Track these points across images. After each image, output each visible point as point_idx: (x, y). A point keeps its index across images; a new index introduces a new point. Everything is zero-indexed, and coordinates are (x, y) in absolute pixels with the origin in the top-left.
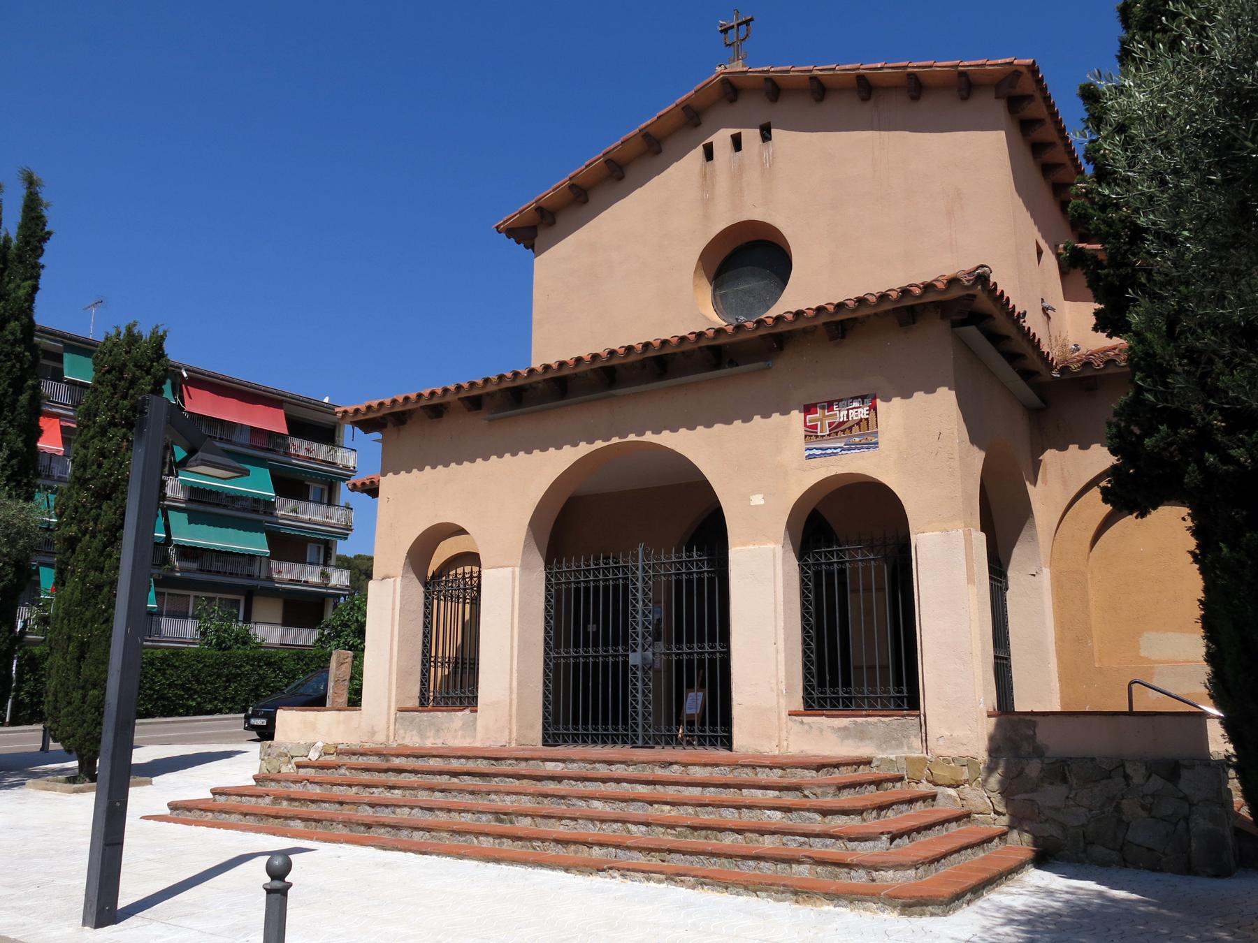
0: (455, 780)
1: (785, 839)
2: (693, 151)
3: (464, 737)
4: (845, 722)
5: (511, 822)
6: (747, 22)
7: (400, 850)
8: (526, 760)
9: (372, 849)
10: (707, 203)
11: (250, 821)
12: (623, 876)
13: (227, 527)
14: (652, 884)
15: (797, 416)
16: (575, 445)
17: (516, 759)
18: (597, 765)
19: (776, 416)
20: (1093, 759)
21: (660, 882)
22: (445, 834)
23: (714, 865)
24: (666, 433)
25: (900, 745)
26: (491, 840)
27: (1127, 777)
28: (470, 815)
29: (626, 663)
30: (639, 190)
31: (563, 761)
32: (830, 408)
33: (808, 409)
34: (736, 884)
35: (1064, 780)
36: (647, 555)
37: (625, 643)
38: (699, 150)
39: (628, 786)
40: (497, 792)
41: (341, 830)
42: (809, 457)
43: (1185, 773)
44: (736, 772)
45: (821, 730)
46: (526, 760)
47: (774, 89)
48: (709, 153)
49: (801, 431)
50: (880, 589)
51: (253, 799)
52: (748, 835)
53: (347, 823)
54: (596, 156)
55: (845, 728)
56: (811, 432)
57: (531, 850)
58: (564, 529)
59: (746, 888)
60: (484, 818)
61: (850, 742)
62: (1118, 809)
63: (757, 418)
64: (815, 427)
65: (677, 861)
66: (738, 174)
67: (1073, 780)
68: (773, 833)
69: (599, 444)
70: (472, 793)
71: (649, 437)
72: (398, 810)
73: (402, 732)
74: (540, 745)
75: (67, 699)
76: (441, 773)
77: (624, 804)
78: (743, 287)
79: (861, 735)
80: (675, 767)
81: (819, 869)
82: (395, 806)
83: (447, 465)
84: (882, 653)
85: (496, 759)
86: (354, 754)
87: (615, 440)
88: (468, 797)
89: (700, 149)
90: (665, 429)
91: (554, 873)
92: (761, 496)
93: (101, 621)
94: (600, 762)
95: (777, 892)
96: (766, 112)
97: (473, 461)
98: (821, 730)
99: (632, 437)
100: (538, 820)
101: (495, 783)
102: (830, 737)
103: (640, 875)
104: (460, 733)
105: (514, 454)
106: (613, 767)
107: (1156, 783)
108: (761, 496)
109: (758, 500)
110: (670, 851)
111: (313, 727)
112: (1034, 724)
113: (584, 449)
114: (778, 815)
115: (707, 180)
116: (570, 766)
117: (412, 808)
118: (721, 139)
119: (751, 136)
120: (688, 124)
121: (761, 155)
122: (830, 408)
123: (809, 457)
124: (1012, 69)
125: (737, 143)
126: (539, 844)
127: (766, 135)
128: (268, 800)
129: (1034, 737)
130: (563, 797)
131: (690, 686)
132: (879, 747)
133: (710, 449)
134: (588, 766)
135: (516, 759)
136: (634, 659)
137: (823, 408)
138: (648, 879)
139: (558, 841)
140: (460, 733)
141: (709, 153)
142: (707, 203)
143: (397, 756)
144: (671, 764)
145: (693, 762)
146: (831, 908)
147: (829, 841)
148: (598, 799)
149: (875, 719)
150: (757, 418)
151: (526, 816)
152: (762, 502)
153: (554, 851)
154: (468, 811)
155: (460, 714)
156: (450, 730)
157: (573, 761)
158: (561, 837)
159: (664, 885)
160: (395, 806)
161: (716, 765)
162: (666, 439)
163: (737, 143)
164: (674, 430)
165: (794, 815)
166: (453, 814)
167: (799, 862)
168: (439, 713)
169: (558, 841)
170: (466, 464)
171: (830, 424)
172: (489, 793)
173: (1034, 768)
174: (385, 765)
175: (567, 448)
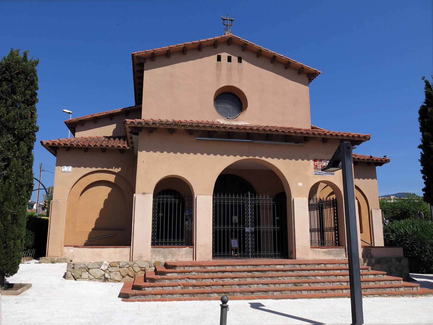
0: (285, 273)
1: (385, 282)
2: (213, 56)
3: (186, 257)
4: (326, 250)
5: (301, 286)
6: (232, 20)
7: (285, 299)
8: (269, 265)
9: (271, 300)
10: (218, 75)
11: (186, 296)
12: (367, 297)
13: (80, 167)
14: (375, 298)
15: (312, 162)
16: (235, 156)
17: (265, 265)
18: (296, 266)
19: (306, 160)
20: (385, 258)
21: (377, 297)
22: (288, 292)
23: (380, 291)
24: (270, 159)
25: (340, 256)
26: (307, 292)
27: (392, 262)
28: (284, 285)
29: (244, 231)
30: (192, 61)
31: (283, 265)
32: (321, 161)
33: (315, 160)
34: (398, 295)
35: (380, 263)
36: (251, 196)
37: (244, 224)
38: (215, 57)
39: (317, 271)
40: (281, 277)
41: (239, 295)
42: (315, 174)
43: (402, 261)
44: (340, 265)
45: (319, 252)
46: (269, 265)
47: (245, 47)
48: (219, 59)
49: (313, 166)
50: (270, 209)
51: (171, 288)
52: (376, 282)
53: (241, 293)
54: (181, 44)
55: (326, 252)
56: (316, 167)
57: (322, 293)
58: (227, 184)
59: (401, 295)
60: (290, 285)
61: (327, 255)
62: (390, 269)
63: (300, 160)
64: (317, 166)
65: (388, 290)
66: (230, 70)
67: (381, 263)
68: (382, 281)
69: (245, 157)
70: (271, 277)
71: (263, 158)
72: (252, 286)
73: (154, 256)
74: (211, 260)
75: (5, 245)
76: (244, 271)
77: (327, 277)
78: (224, 106)
79: (330, 253)
80: (322, 265)
81: (406, 288)
82: (250, 284)
83: (175, 153)
84: (268, 227)
85: (256, 265)
86: (187, 266)
87: (251, 157)
88: (269, 279)
89: (216, 56)
90: (269, 157)
91: (345, 299)
92: (301, 183)
93: (22, 204)
94: (297, 264)
95: (408, 295)
96: (241, 54)
97: (189, 153)
98: (319, 252)
99: (257, 157)
100: (311, 284)
101: (226, 274)
102: (321, 255)
103: (372, 296)
104: (184, 256)
105: (202, 154)
106: (301, 266)
107: (397, 263)
108: (301, 183)
109: (300, 184)
110: (367, 288)
111: (100, 255)
112: (370, 250)
113: (238, 158)
114: (372, 276)
115: (218, 68)
116: (286, 266)
117: (258, 284)
118: (224, 56)
119: (235, 59)
120: (214, 46)
121: (238, 66)
122: (321, 161)
123: (315, 174)
124: (316, 72)
125: (229, 60)
126: (324, 291)
127: (240, 60)
128: (179, 287)
129: (370, 253)
130: (307, 276)
131: (232, 237)
132: (335, 256)
133: (285, 166)
134: (293, 266)
135: (265, 265)
136: (247, 230)
137: (319, 161)
138: (374, 297)
139: (331, 290)
140: (184, 256)
141: (219, 59)
142: (218, 75)
143: (210, 266)
144: (321, 264)
145: (279, 263)
146: (421, 297)
147: (396, 282)
148: (319, 276)
149: (334, 249)
150: (300, 160)
151: (306, 283)
152: (302, 185)
153: (330, 292)
154: (283, 284)
155: (184, 249)
156: (179, 255)
157: (287, 265)
158: (333, 288)
159: (378, 298)
160: (250, 284)
161: (335, 264)
162: (269, 160)
163: (229, 60)
164: (273, 158)
165: (377, 276)
166: (276, 285)
167: (401, 287)
168: (174, 249)
169: (331, 290)
170: (185, 154)
171: (321, 166)
172: (278, 277)
173: (373, 261)
174: (204, 270)
175: (231, 157)
